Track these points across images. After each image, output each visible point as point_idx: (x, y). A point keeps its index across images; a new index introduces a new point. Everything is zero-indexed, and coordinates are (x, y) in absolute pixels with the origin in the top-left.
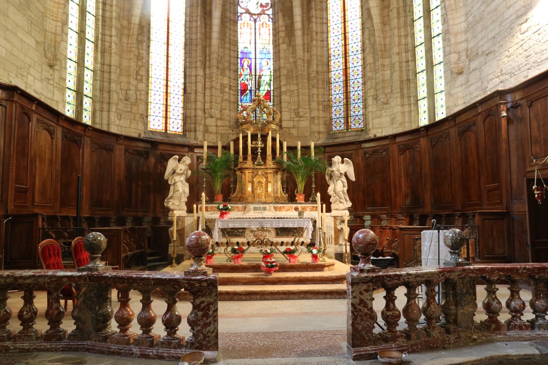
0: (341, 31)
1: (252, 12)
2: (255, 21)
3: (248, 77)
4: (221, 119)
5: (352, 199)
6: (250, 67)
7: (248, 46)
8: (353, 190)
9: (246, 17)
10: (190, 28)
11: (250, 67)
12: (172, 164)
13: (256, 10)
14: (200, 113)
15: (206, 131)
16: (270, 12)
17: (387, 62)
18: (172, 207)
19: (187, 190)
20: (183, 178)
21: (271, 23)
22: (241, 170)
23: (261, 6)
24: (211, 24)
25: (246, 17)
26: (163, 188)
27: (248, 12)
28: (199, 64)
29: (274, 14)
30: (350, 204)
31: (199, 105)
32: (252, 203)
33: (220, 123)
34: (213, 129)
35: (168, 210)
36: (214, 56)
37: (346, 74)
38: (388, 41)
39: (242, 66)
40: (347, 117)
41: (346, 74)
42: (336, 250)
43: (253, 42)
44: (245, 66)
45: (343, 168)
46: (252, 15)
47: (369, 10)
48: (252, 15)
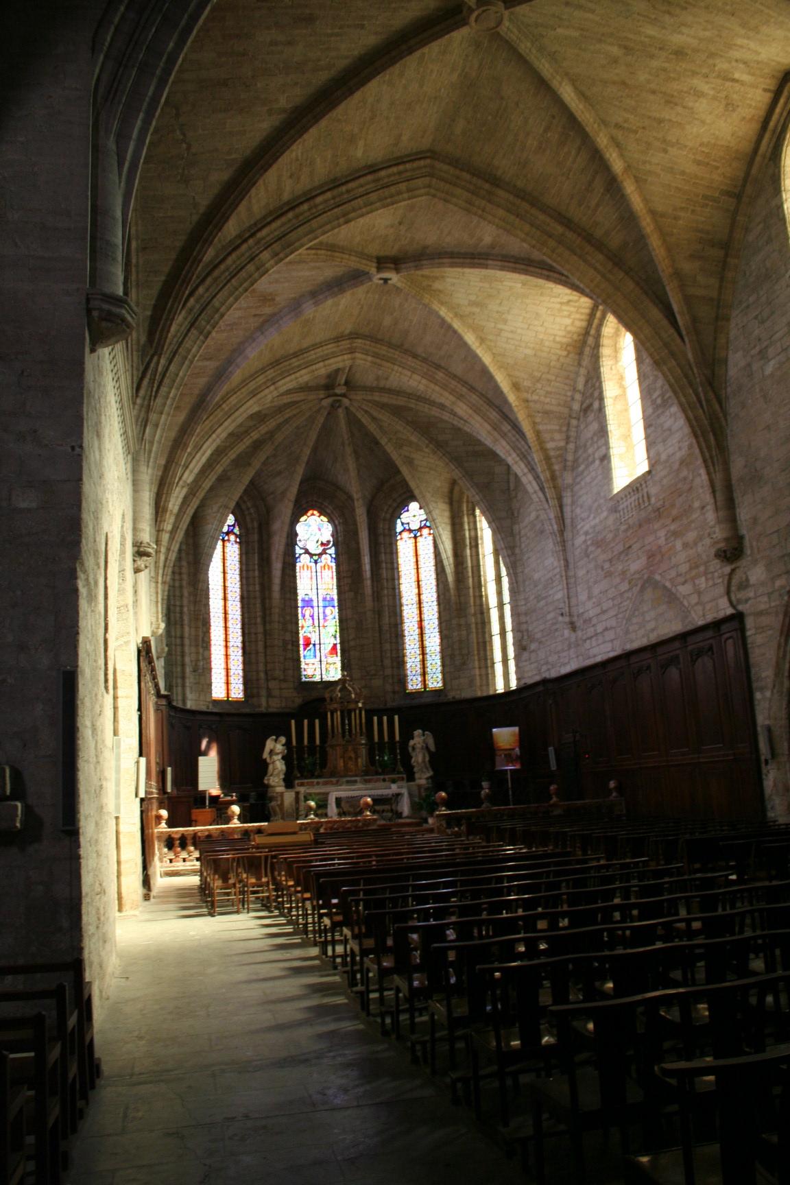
0: (414, 578)
1: (312, 552)
2: (316, 562)
3: (311, 629)
4: (285, 680)
5: (433, 769)
6: (312, 616)
7: (309, 592)
8: (435, 760)
9: (305, 559)
10: (247, 578)
11: (312, 616)
12: (270, 744)
13: (315, 549)
14: (262, 675)
15: (269, 695)
16: (332, 551)
17: (462, 621)
18: (272, 783)
19: (284, 767)
20: (280, 757)
21: (333, 565)
22: (332, 746)
23: (322, 544)
24: (270, 572)
25: (305, 559)
26: (263, 767)
27: (307, 552)
28: (259, 620)
29: (336, 553)
30: (430, 773)
31: (261, 667)
32: (345, 776)
33: (284, 685)
34: (276, 693)
35: (268, 786)
36: (276, 611)
37: (421, 627)
38: (462, 599)
39: (304, 616)
40: (424, 674)
41: (421, 627)
42: (765, 90)
43: (314, 587)
44: (307, 616)
45: (420, 740)
46: (311, 555)
47: (441, 561)
48: (311, 555)
